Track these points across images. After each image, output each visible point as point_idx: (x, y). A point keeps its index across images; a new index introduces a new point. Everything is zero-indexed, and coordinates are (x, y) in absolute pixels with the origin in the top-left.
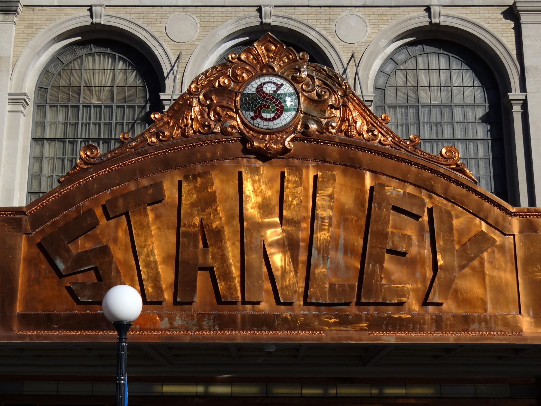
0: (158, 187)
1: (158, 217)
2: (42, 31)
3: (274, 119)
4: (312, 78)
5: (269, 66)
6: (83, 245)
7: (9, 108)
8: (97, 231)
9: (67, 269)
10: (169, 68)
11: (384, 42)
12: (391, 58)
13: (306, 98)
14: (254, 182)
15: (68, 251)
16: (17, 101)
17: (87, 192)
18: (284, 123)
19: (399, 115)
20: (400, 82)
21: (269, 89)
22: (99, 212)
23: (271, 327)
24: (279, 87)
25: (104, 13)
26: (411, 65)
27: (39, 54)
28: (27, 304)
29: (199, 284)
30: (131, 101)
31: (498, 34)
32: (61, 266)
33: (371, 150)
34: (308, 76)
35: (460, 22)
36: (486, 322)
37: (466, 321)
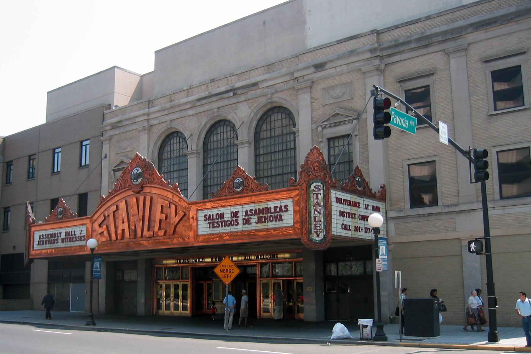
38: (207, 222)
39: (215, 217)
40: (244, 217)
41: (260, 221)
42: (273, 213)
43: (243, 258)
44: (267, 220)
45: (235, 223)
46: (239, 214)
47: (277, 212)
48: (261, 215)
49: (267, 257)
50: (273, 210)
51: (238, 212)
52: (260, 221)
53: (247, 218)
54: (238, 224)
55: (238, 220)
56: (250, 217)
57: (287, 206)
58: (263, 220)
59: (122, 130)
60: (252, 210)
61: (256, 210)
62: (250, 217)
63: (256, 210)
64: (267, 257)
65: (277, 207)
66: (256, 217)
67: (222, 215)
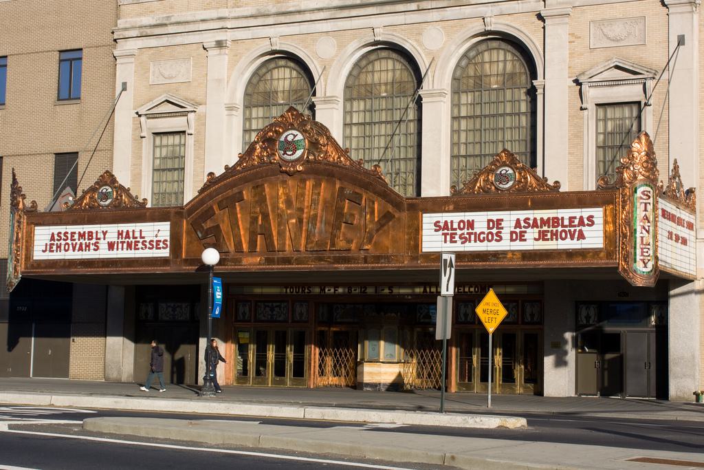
0: (241, 193)
1: (241, 208)
2: (244, 57)
3: (292, 154)
4: (312, 129)
5: (292, 125)
6: (208, 224)
7: (226, 113)
8: (215, 217)
9: (202, 236)
10: (318, 77)
11: (453, 48)
12: (465, 55)
13: (309, 141)
14: (284, 188)
15: (203, 227)
16: (231, 108)
17: (211, 197)
18: (298, 156)
19: (469, 97)
20: (471, 73)
21: (290, 138)
22: (215, 207)
23: (290, 263)
24: (295, 136)
25: (278, 42)
26: (479, 59)
27: (242, 74)
28: (187, 253)
29: (258, 243)
30: (300, 100)
31: (529, 35)
32: (200, 235)
33: (340, 167)
34: (311, 128)
35: (506, 27)
36: (388, 258)
37: (377, 259)
38: (441, 232)
39: (455, 226)
40: (513, 229)
41: (542, 236)
42: (566, 226)
43: (396, 291)
44: (555, 235)
45: (495, 237)
46: (503, 224)
47: (575, 226)
48: (545, 228)
49: (472, 289)
50: (566, 222)
51: (502, 220)
52: (542, 236)
53: (518, 230)
54: (501, 239)
55: (500, 232)
56: (523, 229)
57: (592, 217)
58: (549, 236)
59: (164, 41)
60: (529, 219)
61: (535, 220)
63: (535, 220)
64: (472, 289)
65: (575, 218)
66: (536, 230)
67: (471, 224)
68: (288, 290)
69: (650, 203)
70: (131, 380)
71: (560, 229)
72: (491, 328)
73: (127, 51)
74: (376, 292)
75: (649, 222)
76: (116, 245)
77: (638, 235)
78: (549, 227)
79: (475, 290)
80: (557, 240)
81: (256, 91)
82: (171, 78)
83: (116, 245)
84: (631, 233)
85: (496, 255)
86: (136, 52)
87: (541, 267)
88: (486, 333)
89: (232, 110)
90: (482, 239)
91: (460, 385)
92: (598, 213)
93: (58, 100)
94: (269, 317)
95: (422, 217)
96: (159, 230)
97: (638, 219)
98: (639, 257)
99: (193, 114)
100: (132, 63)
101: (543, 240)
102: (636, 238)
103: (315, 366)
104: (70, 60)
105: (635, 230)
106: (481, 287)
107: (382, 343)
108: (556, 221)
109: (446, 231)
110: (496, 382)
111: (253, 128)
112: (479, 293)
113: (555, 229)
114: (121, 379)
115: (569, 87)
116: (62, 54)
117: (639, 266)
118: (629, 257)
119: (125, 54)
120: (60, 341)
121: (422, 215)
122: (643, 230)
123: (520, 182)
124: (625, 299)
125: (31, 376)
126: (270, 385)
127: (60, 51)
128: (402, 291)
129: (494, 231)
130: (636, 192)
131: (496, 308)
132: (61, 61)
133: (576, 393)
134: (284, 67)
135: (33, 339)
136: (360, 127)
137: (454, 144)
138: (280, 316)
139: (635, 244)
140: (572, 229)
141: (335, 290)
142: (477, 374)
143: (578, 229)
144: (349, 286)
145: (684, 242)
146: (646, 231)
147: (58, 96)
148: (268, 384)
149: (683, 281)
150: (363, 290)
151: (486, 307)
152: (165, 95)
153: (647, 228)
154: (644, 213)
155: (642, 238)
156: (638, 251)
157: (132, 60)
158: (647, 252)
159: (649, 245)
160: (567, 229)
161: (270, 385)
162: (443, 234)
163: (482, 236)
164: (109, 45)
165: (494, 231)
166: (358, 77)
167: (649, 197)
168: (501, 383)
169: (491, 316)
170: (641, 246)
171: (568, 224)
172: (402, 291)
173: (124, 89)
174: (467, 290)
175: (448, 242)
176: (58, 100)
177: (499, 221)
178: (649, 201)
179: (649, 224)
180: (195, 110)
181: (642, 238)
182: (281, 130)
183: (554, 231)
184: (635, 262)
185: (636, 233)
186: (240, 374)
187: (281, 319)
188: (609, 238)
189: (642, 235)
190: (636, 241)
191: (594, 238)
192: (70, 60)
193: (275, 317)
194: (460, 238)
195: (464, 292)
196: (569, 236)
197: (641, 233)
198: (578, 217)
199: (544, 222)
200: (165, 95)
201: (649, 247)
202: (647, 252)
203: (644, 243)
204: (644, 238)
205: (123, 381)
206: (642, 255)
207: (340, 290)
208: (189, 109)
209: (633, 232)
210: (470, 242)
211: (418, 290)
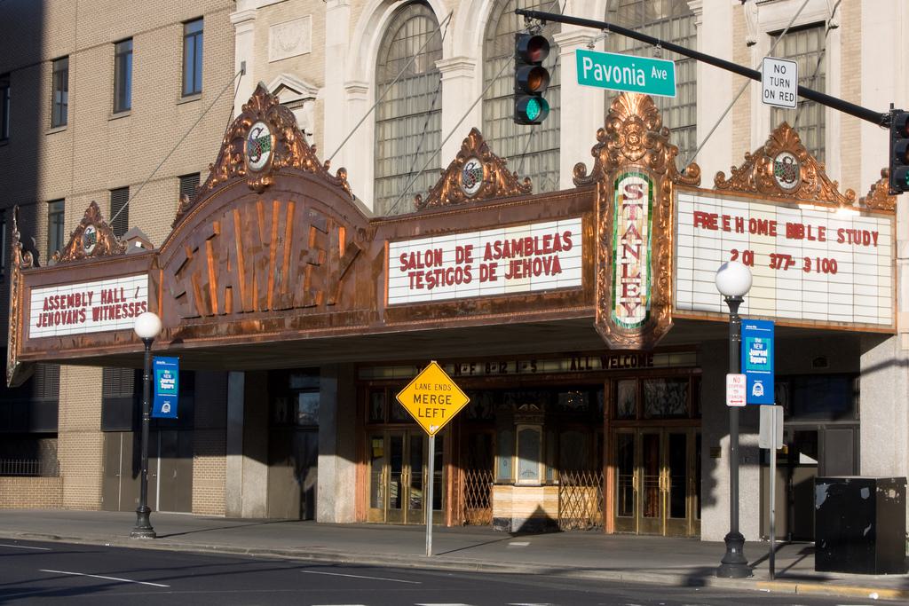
7: (349, 96)
24: (260, 131)
36: (352, 317)
38: (408, 271)
48: (518, 257)
53: (488, 262)
56: (494, 261)
62: (494, 261)
64: (629, 362)
67: (437, 256)
68: (622, 362)
69: (641, 206)
70: (262, 514)
71: (533, 257)
72: (432, 426)
73: (245, 14)
74: (517, 371)
75: (639, 237)
76: (108, 315)
77: (619, 261)
78: (521, 256)
79: (632, 361)
80: (530, 276)
81: (390, 58)
82: (290, 49)
83: (108, 315)
84: (610, 258)
85: (464, 306)
86: (256, 14)
87: (510, 322)
88: (421, 436)
89: (353, 92)
90: (450, 279)
91: (618, 522)
92: (574, 226)
93: (184, 96)
94: (663, 408)
95: (389, 249)
96: (138, 288)
97: (619, 233)
98: (619, 300)
99: (311, 102)
100: (251, 31)
101: (490, 280)
102: (615, 265)
103: (454, 492)
104: (193, 30)
105: (615, 253)
106: (639, 356)
107: (517, 459)
108: (527, 245)
109: (412, 270)
110: (662, 516)
111: (387, 118)
112: (637, 367)
113: (527, 258)
114: (240, 514)
115: (735, 7)
116: (188, 26)
117: (620, 315)
118: (608, 302)
119: (245, 18)
120: (185, 461)
121: (388, 245)
122: (636, 250)
123: (488, 182)
124: (823, 370)
125: (157, 509)
126: (405, 523)
127: (185, 23)
128: (550, 367)
129: (463, 265)
130: (616, 187)
131: (445, 393)
132: (185, 37)
133: (761, 537)
134: (420, 16)
135: (159, 460)
136: (505, 102)
137: (378, 161)
138: (678, 407)
139: (615, 277)
140: (547, 256)
141: (472, 369)
142: (665, 505)
143: (553, 255)
144: (486, 361)
145: (830, 266)
146: (633, 253)
147: (183, 90)
148: (403, 521)
149: (877, 337)
150: (503, 367)
151: (422, 392)
152: (280, 76)
153: (635, 249)
154: (629, 223)
155: (625, 266)
156: (619, 289)
157: (250, 26)
158: (634, 290)
159: (638, 277)
160: (541, 257)
161: (405, 523)
162: (411, 275)
163: (451, 274)
164: (229, 7)
165: (463, 265)
166: (499, 24)
167: (640, 195)
168: (669, 517)
169: (432, 406)
170: (624, 281)
171: (542, 248)
172: (550, 367)
173: (243, 72)
174: (583, 364)
175: (415, 287)
176: (184, 96)
177: (469, 247)
178: (639, 202)
179: (639, 242)
180: (312, 96)
181: (625, 266)
182: (249, 124)
183: (547, 259)
184: (614, 308)
185: (615, 258)
186: (392, 505)
187: (679, 411)
188: (588, 271)
189: (624, 261)
190: (615, 272)
191: (571, 274)
192: (193, 30)
193: (671, 408)
194: (428, 280)
195: (619, 366)
196: (543, 269)
197: (624, 257)
198: (553, 236)
199: (518, 247)
200: (280, 76)
201: (638, 281)
202: (634, 290)
203: (629, 274)
204: (629, 266)
205: (243, 515)
206: (625, 295)
207: (478, 369)
208: (305, 95)
209: (613, 256)
210: (437, 286)
211: (566, 365)
